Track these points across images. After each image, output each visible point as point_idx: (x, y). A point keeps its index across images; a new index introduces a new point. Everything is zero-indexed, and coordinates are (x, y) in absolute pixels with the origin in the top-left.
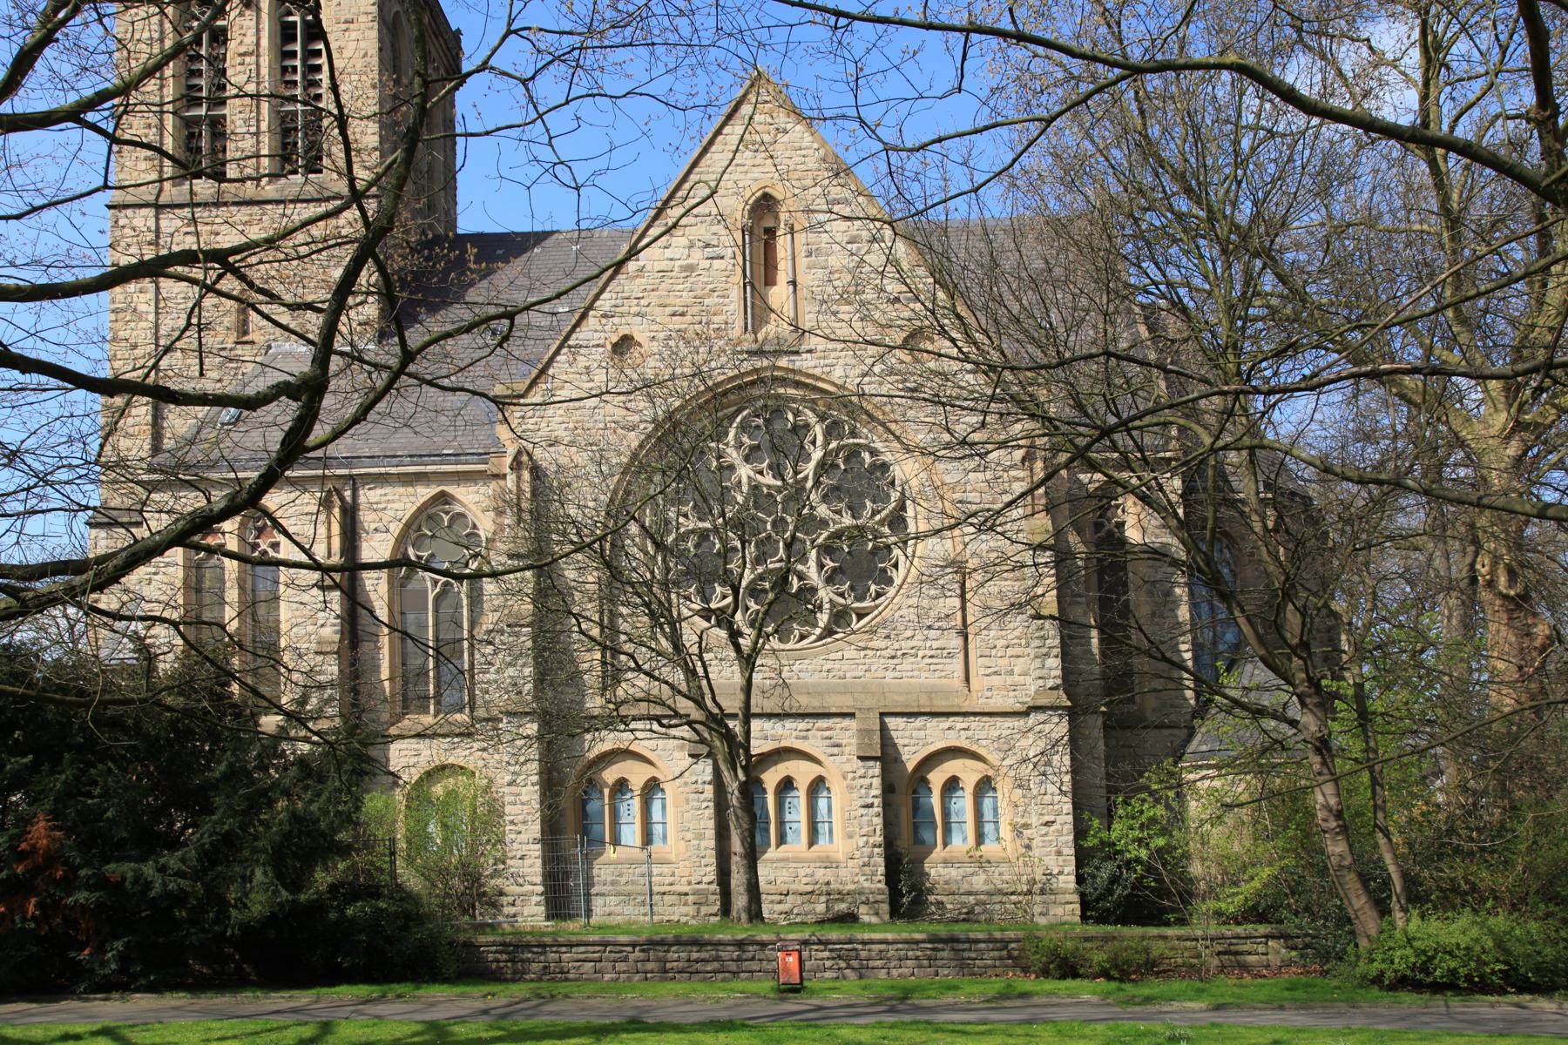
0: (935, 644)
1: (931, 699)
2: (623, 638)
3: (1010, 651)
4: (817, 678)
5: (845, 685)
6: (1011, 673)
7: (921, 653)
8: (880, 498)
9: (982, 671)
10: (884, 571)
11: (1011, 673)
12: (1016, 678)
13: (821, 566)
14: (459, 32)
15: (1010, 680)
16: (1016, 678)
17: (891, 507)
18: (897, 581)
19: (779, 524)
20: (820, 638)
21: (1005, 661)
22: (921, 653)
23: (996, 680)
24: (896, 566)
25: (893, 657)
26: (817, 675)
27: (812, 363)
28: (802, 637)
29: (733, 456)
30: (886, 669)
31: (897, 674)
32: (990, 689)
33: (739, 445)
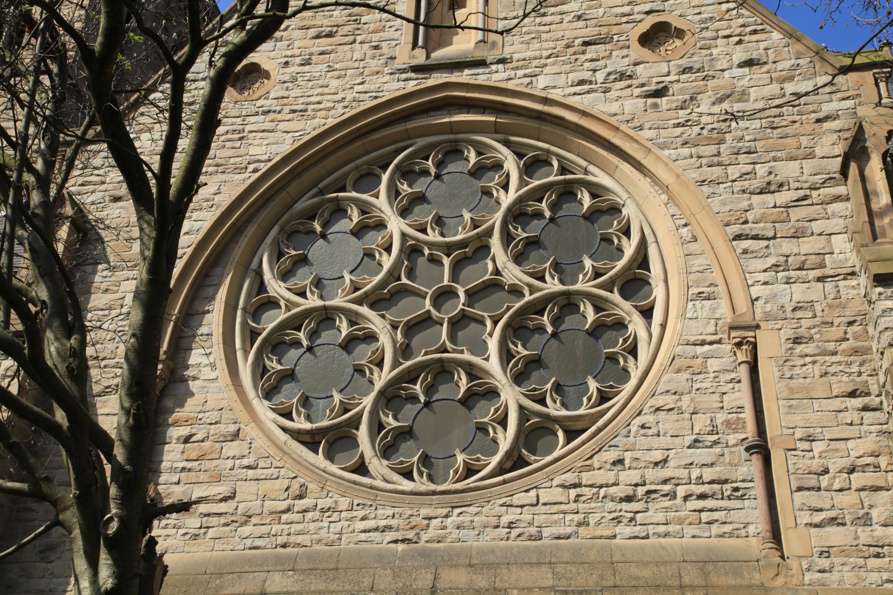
0: (708, 474)
1: (706, 575)
2: (133, 23)
3: (858, 480)
4: (490, 539)
5: (540, 551)
6: (866, 520)
7: (681, 491)
8: (607, 247)
9: (805, 518)
10: (612, 358)
11: (866, 520)
12: (879, 531)
13: (506, 355)
14: (167, 566)
15: (864, 535)
16: (879, 531)
17: (620, 264)
18: (635, 376)
19: (444, 296)
20: (501, 470)
21: (847, 500)
22: (681, 491)
23: (835, 536)
24: (633, 351)
25: (629, 499)
26: (491, 533)
27: (504, 75)
28: (470, 471)
29: (382, 203)
30: (617, 520)
31: (637, 530)
32: (825, 553)
33: (394, 193)
